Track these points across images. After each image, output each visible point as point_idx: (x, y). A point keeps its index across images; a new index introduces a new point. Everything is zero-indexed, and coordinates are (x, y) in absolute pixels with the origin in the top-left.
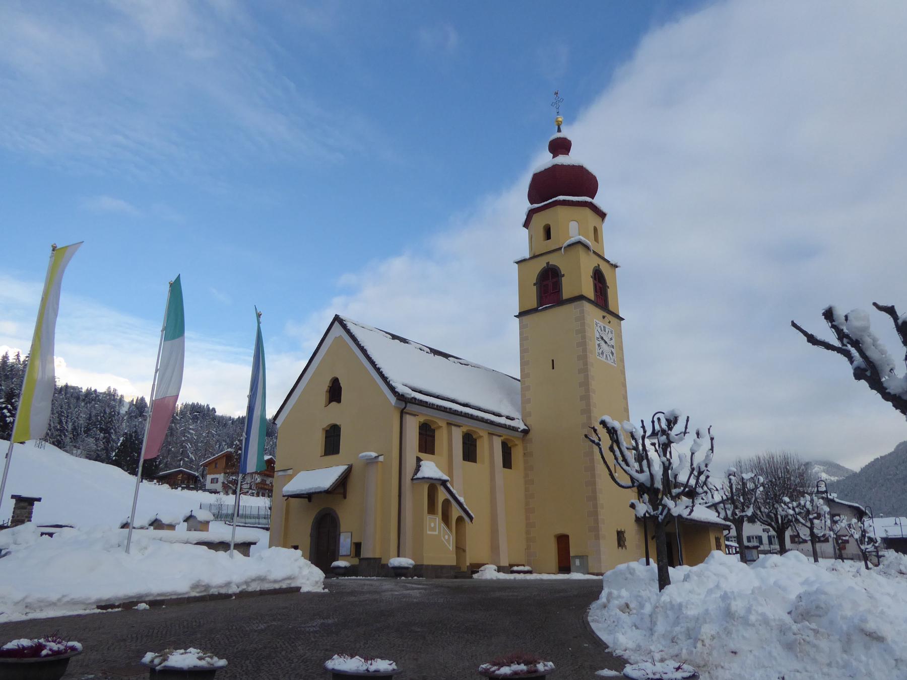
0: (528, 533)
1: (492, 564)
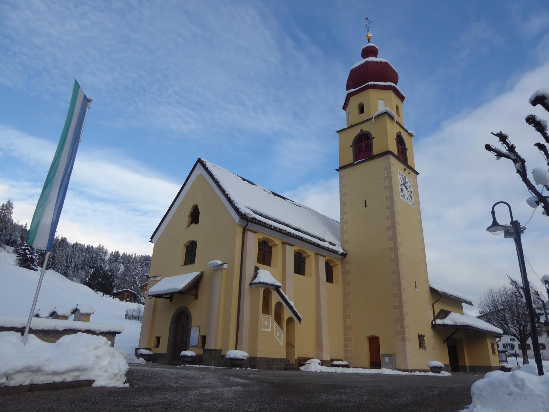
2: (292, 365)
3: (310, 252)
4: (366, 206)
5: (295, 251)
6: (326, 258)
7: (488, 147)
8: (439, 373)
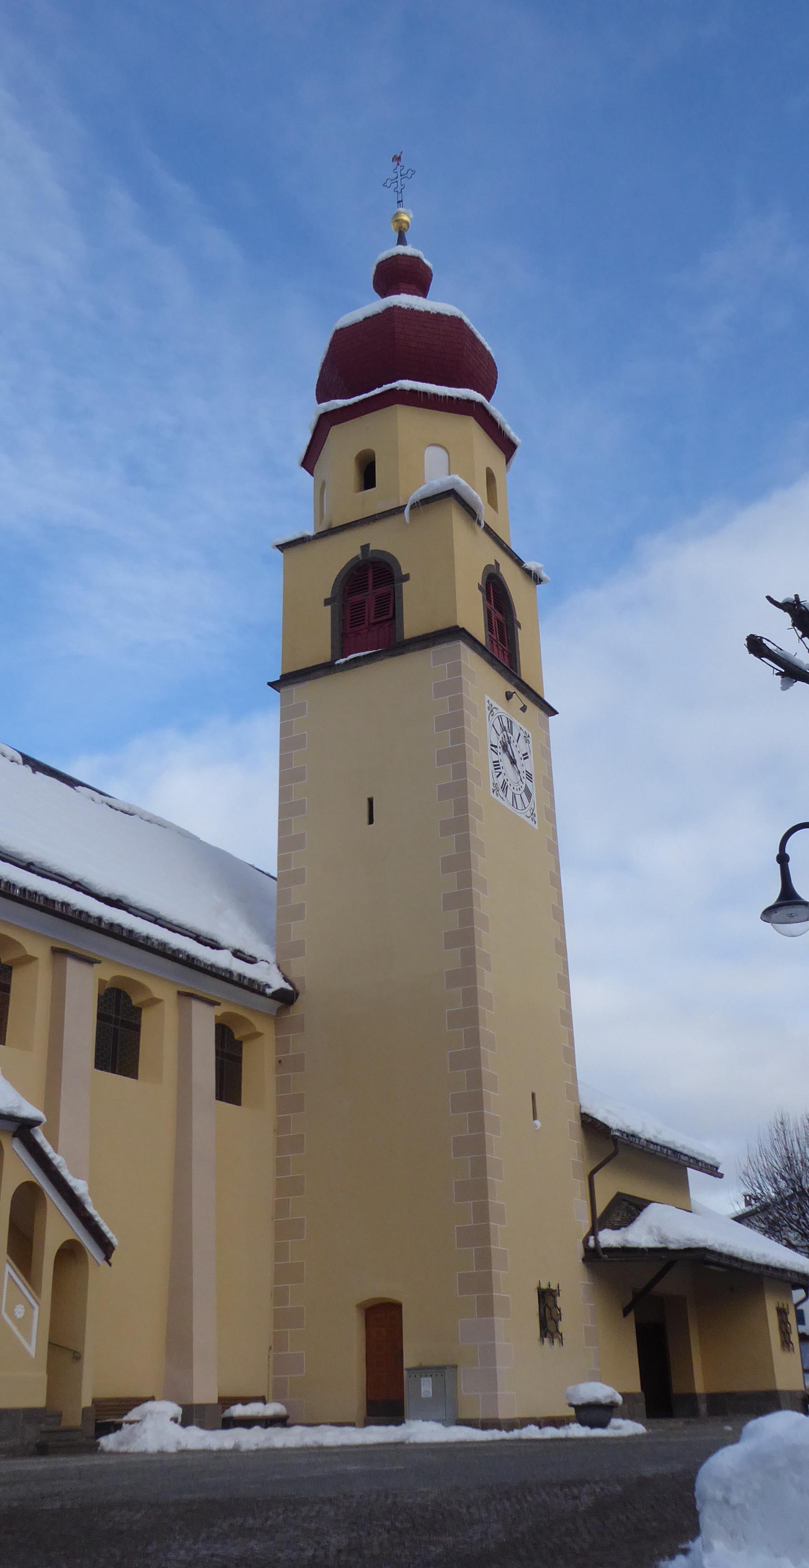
0: (279, 1297)
1: (171, 1400)
2: (70, 1430)
3: (160, 987)
4: (371, 821)
5: (101, 982)
6: (219, 1011)
7: (756, 646)
8: (604, 1425)
